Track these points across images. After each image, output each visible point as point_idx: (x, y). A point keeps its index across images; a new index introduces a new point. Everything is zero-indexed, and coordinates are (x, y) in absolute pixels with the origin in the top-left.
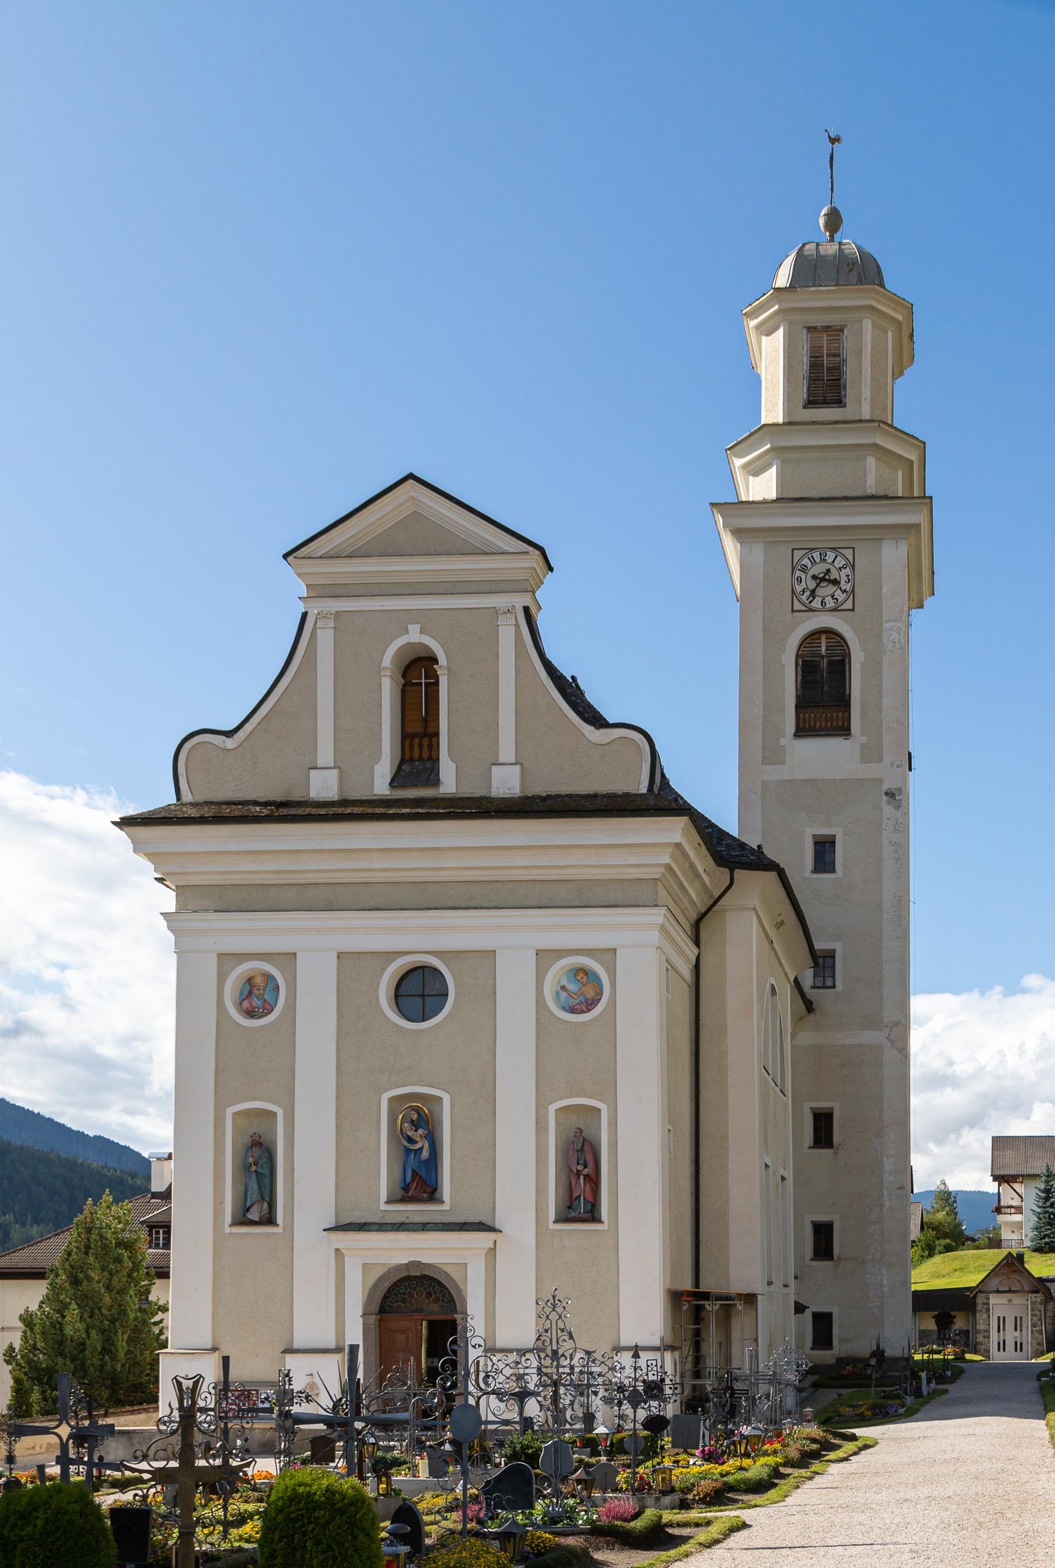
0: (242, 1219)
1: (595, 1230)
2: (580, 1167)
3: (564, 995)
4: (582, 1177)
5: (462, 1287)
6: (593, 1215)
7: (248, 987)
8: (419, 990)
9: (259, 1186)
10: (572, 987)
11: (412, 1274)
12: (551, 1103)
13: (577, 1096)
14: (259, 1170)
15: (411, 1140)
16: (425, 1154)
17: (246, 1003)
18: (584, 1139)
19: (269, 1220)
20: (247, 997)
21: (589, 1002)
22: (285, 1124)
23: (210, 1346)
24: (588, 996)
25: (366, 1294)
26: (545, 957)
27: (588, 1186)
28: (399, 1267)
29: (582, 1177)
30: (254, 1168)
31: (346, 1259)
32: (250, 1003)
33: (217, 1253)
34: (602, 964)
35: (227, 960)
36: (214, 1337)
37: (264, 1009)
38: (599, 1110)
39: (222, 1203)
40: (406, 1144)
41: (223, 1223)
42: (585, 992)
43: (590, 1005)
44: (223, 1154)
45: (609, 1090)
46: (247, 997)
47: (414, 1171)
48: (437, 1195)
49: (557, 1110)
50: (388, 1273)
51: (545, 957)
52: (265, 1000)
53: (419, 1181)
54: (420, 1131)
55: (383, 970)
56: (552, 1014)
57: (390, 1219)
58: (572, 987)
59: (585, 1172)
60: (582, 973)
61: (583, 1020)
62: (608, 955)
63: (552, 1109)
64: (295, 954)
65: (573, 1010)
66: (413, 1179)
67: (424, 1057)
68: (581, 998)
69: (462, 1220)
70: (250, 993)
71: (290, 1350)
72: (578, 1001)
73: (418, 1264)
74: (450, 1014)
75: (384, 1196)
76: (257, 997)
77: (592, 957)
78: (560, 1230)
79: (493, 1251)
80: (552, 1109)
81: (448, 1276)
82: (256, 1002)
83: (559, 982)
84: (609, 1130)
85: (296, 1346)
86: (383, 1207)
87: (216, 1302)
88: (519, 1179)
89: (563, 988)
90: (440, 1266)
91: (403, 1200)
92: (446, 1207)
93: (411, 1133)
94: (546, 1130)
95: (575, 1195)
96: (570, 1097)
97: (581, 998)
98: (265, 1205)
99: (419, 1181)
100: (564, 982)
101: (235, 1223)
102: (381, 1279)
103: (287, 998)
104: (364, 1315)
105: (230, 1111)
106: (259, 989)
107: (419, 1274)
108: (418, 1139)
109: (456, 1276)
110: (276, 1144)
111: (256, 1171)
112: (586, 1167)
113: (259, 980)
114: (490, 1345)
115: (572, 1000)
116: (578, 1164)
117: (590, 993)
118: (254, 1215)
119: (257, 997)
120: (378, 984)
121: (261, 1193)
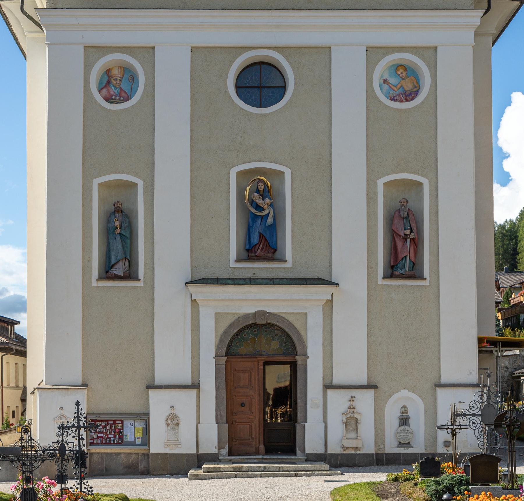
0: (107, 273)
1: (419, 286)
2: (408, 232)
3: (386, 87)
4: (408, 240)
5: (302, 333)
6: (415, 273)
7: (106, 78)
8: (261, 82)
9: (123, 246)
10: (393, 81)
11: (259, 321)
12: (379, 178)
13: (402, 171)
14: (123, 232)
15: (258, 208)
16: (270, 220)
17: (104, 91)
18: (409, 210)
19: (130, 275)
20: (105, 86)
21: (408, 93)
22: (145, 193)
23: (80, 382)
24: (407, 88)
25: (218, 338)
26: (374, 53)
27: (412, 248)
28: (247, 316)
29: (408, 240)
30: (118, 231)
31: (200, 307)
32: (108, 91)
33: (86, 304)
34: (424, 59)
35: (93, 52)
36: (83, 375)
37: (120, 97)
38: (283, 173)
39: (90, 260)
40: (253, 211)
41: (91, 278)
42: (406, 85)
43: (410, 95)
44: (90, 218)
45: (431, 167)
46: (105, 86)
47: (260, 234)
48: (277, 255)
49: (385, 184)
50: (238, 320)
51: (374, 53)
52: (121, 89)
53: (261, 241)
54: (268, 200)
55: (231, 62)
56: (380, 102)
57: (238, 275)
58: (393, 81)
59: (412, 235)
60: (403, 69)
61: (138, 98)
62: (430, 53)
63: (381, 182)
64: (436, 48)
65: (393, 99)
66: (260, 241)
67: (267, 136)
68: (401, 90)
69: (302, 276)
70: (109, 82)
71: (151, 386)
72: (397, 93)
73: (264, 313)
74: (290, 101)
75: (233, 255)
76: (117, 85)
77: (415, 54)
78: (388, 286)
79: (330, 303)
80: (381, 182)
81: (290, 324)
82: (113, 90)
83: (382, 77)
84: (430, 201)
85: (157, 383)
86: (233, 265)
87: (85, 346)
88: (353, 243)
89: (385, 81)
90: (283, 316)
91: (250, 259)
92: (289, 265)
93: (259, 202)
94: (376, 201)
95: (400, 256)
96: (396, 172)
97: (401, 90)
98: (127, 263)
99: (261, 241)
100: (386, 76)
101: (100, 278)
102: (231, 326)
103: (146, 86)
104: (216, 356)
105: (96, 182)
106: (116, 80)
107: (265, 322)
108: (265, 207)
109: (297, 324)
110: (137, 211)
111: (120, 234)
112: (412, 231)
113: (116, 72)
114: (328, 382)
115: (392, 92)
116: (405, 230)
117: (408, 86)
118: (119, 270)
119: (117, 85)
120: (227, 75)
121: (125, 253)
